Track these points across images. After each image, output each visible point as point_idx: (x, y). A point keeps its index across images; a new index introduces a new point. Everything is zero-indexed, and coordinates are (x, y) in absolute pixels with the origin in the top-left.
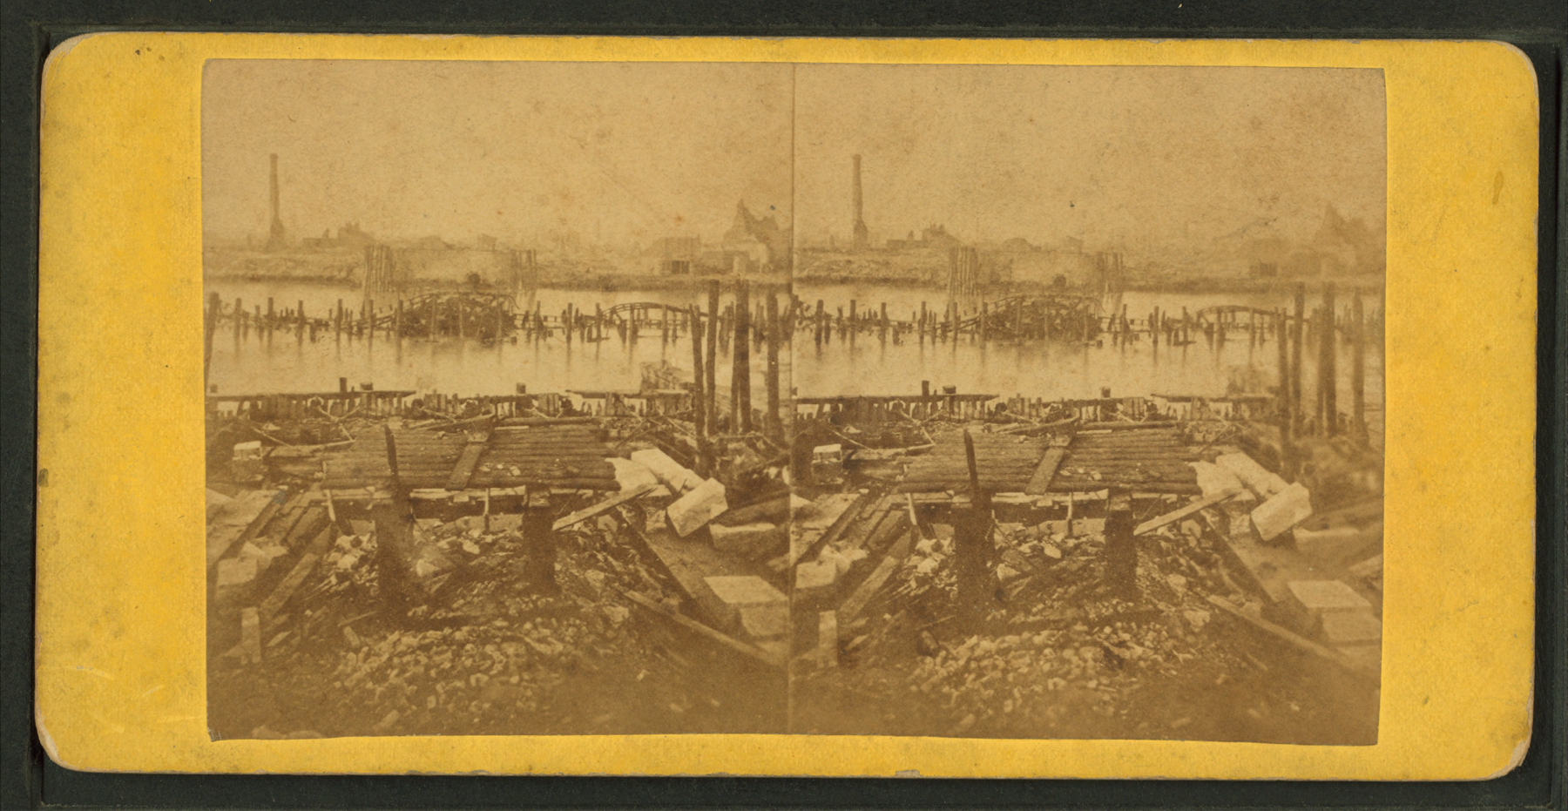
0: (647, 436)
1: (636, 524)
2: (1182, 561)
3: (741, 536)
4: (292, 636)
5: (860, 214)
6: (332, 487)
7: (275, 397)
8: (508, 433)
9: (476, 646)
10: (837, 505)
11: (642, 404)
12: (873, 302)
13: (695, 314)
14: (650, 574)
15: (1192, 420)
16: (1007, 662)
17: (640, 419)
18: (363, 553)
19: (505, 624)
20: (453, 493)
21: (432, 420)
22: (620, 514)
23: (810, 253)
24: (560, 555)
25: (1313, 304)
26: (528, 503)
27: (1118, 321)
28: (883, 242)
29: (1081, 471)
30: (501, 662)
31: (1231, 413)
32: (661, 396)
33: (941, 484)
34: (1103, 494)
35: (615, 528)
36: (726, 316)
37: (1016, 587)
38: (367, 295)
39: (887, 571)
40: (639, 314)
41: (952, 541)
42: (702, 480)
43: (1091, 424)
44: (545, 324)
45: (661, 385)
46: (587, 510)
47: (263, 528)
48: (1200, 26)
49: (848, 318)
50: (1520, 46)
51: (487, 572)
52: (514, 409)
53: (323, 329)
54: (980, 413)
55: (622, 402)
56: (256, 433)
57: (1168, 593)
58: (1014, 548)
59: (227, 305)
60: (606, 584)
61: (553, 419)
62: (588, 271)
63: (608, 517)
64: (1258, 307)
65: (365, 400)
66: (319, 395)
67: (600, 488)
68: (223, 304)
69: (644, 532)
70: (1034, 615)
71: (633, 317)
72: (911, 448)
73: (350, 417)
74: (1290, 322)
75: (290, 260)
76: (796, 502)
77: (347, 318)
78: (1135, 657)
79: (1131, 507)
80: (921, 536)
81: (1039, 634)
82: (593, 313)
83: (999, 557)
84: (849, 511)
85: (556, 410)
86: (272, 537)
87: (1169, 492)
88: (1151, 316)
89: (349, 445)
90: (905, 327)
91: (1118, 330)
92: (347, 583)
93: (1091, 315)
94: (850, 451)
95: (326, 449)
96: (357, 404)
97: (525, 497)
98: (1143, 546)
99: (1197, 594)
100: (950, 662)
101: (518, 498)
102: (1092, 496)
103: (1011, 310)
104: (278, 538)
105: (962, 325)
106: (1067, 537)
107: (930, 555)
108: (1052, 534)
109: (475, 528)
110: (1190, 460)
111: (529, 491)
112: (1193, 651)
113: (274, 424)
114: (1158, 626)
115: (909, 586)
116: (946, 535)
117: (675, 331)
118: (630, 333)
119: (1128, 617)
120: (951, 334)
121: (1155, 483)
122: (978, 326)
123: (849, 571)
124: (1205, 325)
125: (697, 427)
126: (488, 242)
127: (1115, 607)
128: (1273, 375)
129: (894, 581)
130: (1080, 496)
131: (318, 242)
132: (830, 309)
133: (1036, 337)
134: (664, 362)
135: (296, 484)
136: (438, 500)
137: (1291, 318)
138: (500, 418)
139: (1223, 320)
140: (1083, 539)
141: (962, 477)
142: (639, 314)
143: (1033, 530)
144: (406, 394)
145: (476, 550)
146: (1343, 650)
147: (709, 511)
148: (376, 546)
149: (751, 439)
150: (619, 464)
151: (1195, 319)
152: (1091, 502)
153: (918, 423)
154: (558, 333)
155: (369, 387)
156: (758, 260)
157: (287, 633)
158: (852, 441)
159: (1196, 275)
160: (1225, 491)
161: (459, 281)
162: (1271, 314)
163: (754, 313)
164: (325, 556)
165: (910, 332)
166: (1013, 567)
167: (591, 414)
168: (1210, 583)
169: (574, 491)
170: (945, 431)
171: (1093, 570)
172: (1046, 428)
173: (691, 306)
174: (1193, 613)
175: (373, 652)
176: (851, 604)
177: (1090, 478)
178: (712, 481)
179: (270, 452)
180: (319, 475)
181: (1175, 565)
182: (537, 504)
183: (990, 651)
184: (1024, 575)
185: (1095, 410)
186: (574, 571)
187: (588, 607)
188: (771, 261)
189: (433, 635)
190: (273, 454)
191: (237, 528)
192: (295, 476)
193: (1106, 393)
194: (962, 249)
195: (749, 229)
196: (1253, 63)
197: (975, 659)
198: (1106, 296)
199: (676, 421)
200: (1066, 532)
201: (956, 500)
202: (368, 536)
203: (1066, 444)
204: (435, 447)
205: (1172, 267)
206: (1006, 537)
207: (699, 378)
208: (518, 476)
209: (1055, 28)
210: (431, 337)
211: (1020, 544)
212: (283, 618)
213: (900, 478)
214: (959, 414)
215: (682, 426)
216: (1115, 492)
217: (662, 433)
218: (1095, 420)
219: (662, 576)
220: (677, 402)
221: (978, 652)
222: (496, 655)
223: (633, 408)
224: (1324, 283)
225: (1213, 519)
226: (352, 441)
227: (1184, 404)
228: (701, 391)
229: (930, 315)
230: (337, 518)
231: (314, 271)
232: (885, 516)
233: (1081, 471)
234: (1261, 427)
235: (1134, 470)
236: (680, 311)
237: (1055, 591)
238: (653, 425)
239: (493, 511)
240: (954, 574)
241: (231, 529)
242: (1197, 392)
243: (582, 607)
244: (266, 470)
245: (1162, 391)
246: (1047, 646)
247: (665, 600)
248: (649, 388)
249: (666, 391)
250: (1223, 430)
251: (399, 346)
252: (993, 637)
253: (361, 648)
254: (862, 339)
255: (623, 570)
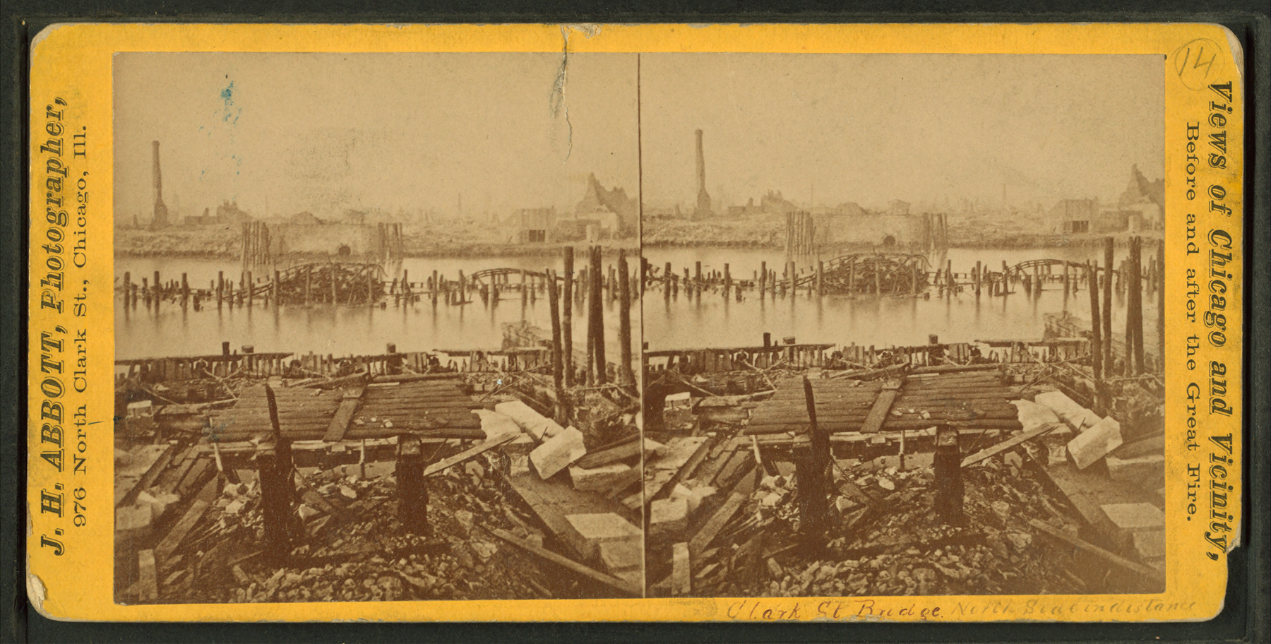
0: (511, 390)
1: (1039, 458)
2: (1005, 489)
3: (601, 477)
4: (721, 567)
5: (160, 194)
6: (218, 441)
7: (164, 361)
8: (380, 389)
9: (355, 581)
10: (686, 447)
11: (504, 360)
12: (714, 263)
13: (553, 278)
14: (1053, 504)
15: (471, 372)
16: (847, 584)
17: (1043, 364)
18: (249, 499)
19: (917, 552)
20: (330, 444)
21: (851, 370)
22: (1025, 450)
23: (657, 220)
24: (431, 498)
25: (581, 264)
26: (400, 453)
27: (943, 275)
28: (181, 217)
29: (912, 411)
30: (912, 586)
31: (507, 365)
32: (522, 353)
33: (783, 426)
34: (932, 431)
35: (481, 473)
36: (581, 279)
37: (316, 524)
38: (789, 255)
39: (198, 512)
40: (499, 279)
41: (794, 476)
42: (562, 428)
43: (379, 378)
44: (955, 280)
45: (522, 343)
46: (456, 456)
47: (158, 478)
48: (958, 12)
49: (694, 279)
50: (1224, 24)
51: (901, 506)
52: (927, 358)
53: (748, 289)
54: (276, 369)
55: (486, 359)
56: (686, 385)
57: (993, 520)
58: (851, 481)
59: (658, 269)
60: (1011, 514)
61: (963, 366)
62: (451, 241)
63: (1013, 453)
64: (528, 269)
65: (246, 363)
66: (745, 349)
67: (1006, 428)
68: (654, 268)
69: (1047, 466)
70: (335, 550)
71: (494, 282)
72: (755, 394)
73: (773, 369)
74: (1100, 273)
75: (716, 226)
76: (651, 445)
77: (227, 288)
78: (963, 576)
79: (958, 441)
80: (227, 481)
81: (875, 558)
82: (456, 278)
83: (300, 497)
84: (161, 459)
85: (966, 358)
86: (702, 479)
87: (452, 436)
88: (973, 270)
89: (233, 403)
90: (746, 285)
91: (944, 283)
92: (235, 526)
93: (919, 270)
94: (159, 407)
95: (213, 407)
96: (780, 357)
97: (398, 447)
98: (970, 478)
99: (1018, 517)
100: (794, 586)
101: (390, 448)
102: (923, 432)
103: (301, 277)
104: (170, 488)
105: (800, 282)
106: (899, 471)
107: (236, 497)
108: (885, 468)
109: (352, 475)
110: (1010, 399)
111: (401, 441)
112: (1016, 569)
113: (164, 385)
114: (449, 558)
115: (755, 518)
116: (788, 470)
117: (533, 293)
118: (1034, 288)
119: (955, 541)
120: (789, 291)
121: (444, 429)
122: (814, 283)
123: (165, 512)
124: (480, 287)
125: (556, 380)
126: (903, 209)
127: (409, 541)
128: (1084, 319)
129: (742, 513)
130: (370, 442)
131: (199, 219)
132: (677, 270)
133: (868, 292)
134: (1065, 313)
135: (186, 438)
136: (317, 450)
137: (1102, 269)
138: (373, 375)
139: (1039, 273)
140: (914, 472)
141: (265, 427)
142: (499, 279)
143: (868, 465)
144: (284, 356)
145: (353, 494)
146: (620, 575)
147: (569, 456)
148: (261, 492)
149: (606, 389)
150: (484, 415)
151: (1014, 272)
152: (381, 447)
153: (762, 371)
154: (967, 289)
155: (792, 341)
156: (1152, 218)
157: (715, 565)
158: (161, 398)
159: (1015, 233)
160: (1044, 425)
161: (330, 253)
162: (542, 275)
163: (607, 277)
164: (752, 494)
165: (209, 300)
166: (313, 507)
167: (457, 371)
168: (494, 518)
169: (442, 440)
170: (786, 378)
171: (923, 499)
172: (338, 382)
173: (547, 270)
174: (1015, 535)
175: (260, 588)
176: (704, 536)
177: (920, 417)
178: (571, 428)
179: (699, 402)
180: (207, 430)
181: (462, 502)
182: (409, 452)
183: (831, 575)
184: (323, 513)
185: (924, 355)
186: (445, 512)
187: (993, 534)
188: (622, 229)
189: (850, 564)
190: (163, 412)
191: (668, 472)
192: (722, 423)
193: (392, 348)
194: (799, 213)
195: (601, 202)
196: (433, 48)
197: (283, 590)
198: (932, 253)
199: (1076, 365)
200: (899, 465)
201: (797, 439)
202: (253, 483)
203: (897, 387)
204: (312, 403)
205: (447, 235)
206: (843, 472)
207: (1096, 327)
208: (928, 419)
209: (841, 14)
210: (306, 304)
211: (856, 478)
212: (711, 552)
213: (745, 422)
214: (257, 371)
215: (1081, 370)
216: (942, 428)
217: (523, 386)
218: (924, 365)
219: (526, 515)
220: (536, 359)
221: (820, 576)
222: (908, 580)
223: (1036, 355)
224: (1131, 238)
225: (1033, 451)
226: (235, 399)
227: (1004, 348)
228: (559, 346)
229: (770, 274)
230: (224, 469)
231: (740, 236)
232: (194, 463)
233: (912, 411)
234: (537, 376)
235: (422, 418)
236: (1080, 266)
237: (352, 529)
238: (514, 379)
239: (369, 459)
240: (796, 507)
241: (661, 473)
242: (1015, 338)
243: (988, 535)
244: (695, 419)
245: (439, 348)
246: (347, 577)
247: (530, 537)
248: (1051, 336)
249: (1067, 339)
250: (1040, 371)
251: (820, 303)
252: (297, 570)
253: (250, 584)
254: (165, 306)
255: (1027, 501)
